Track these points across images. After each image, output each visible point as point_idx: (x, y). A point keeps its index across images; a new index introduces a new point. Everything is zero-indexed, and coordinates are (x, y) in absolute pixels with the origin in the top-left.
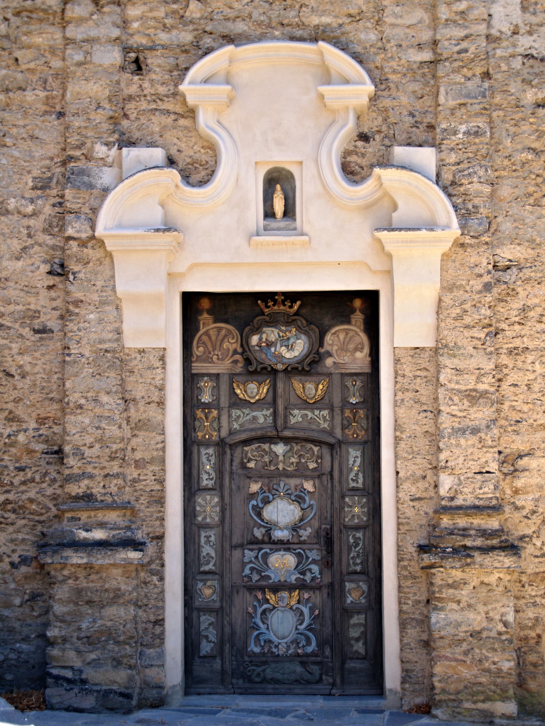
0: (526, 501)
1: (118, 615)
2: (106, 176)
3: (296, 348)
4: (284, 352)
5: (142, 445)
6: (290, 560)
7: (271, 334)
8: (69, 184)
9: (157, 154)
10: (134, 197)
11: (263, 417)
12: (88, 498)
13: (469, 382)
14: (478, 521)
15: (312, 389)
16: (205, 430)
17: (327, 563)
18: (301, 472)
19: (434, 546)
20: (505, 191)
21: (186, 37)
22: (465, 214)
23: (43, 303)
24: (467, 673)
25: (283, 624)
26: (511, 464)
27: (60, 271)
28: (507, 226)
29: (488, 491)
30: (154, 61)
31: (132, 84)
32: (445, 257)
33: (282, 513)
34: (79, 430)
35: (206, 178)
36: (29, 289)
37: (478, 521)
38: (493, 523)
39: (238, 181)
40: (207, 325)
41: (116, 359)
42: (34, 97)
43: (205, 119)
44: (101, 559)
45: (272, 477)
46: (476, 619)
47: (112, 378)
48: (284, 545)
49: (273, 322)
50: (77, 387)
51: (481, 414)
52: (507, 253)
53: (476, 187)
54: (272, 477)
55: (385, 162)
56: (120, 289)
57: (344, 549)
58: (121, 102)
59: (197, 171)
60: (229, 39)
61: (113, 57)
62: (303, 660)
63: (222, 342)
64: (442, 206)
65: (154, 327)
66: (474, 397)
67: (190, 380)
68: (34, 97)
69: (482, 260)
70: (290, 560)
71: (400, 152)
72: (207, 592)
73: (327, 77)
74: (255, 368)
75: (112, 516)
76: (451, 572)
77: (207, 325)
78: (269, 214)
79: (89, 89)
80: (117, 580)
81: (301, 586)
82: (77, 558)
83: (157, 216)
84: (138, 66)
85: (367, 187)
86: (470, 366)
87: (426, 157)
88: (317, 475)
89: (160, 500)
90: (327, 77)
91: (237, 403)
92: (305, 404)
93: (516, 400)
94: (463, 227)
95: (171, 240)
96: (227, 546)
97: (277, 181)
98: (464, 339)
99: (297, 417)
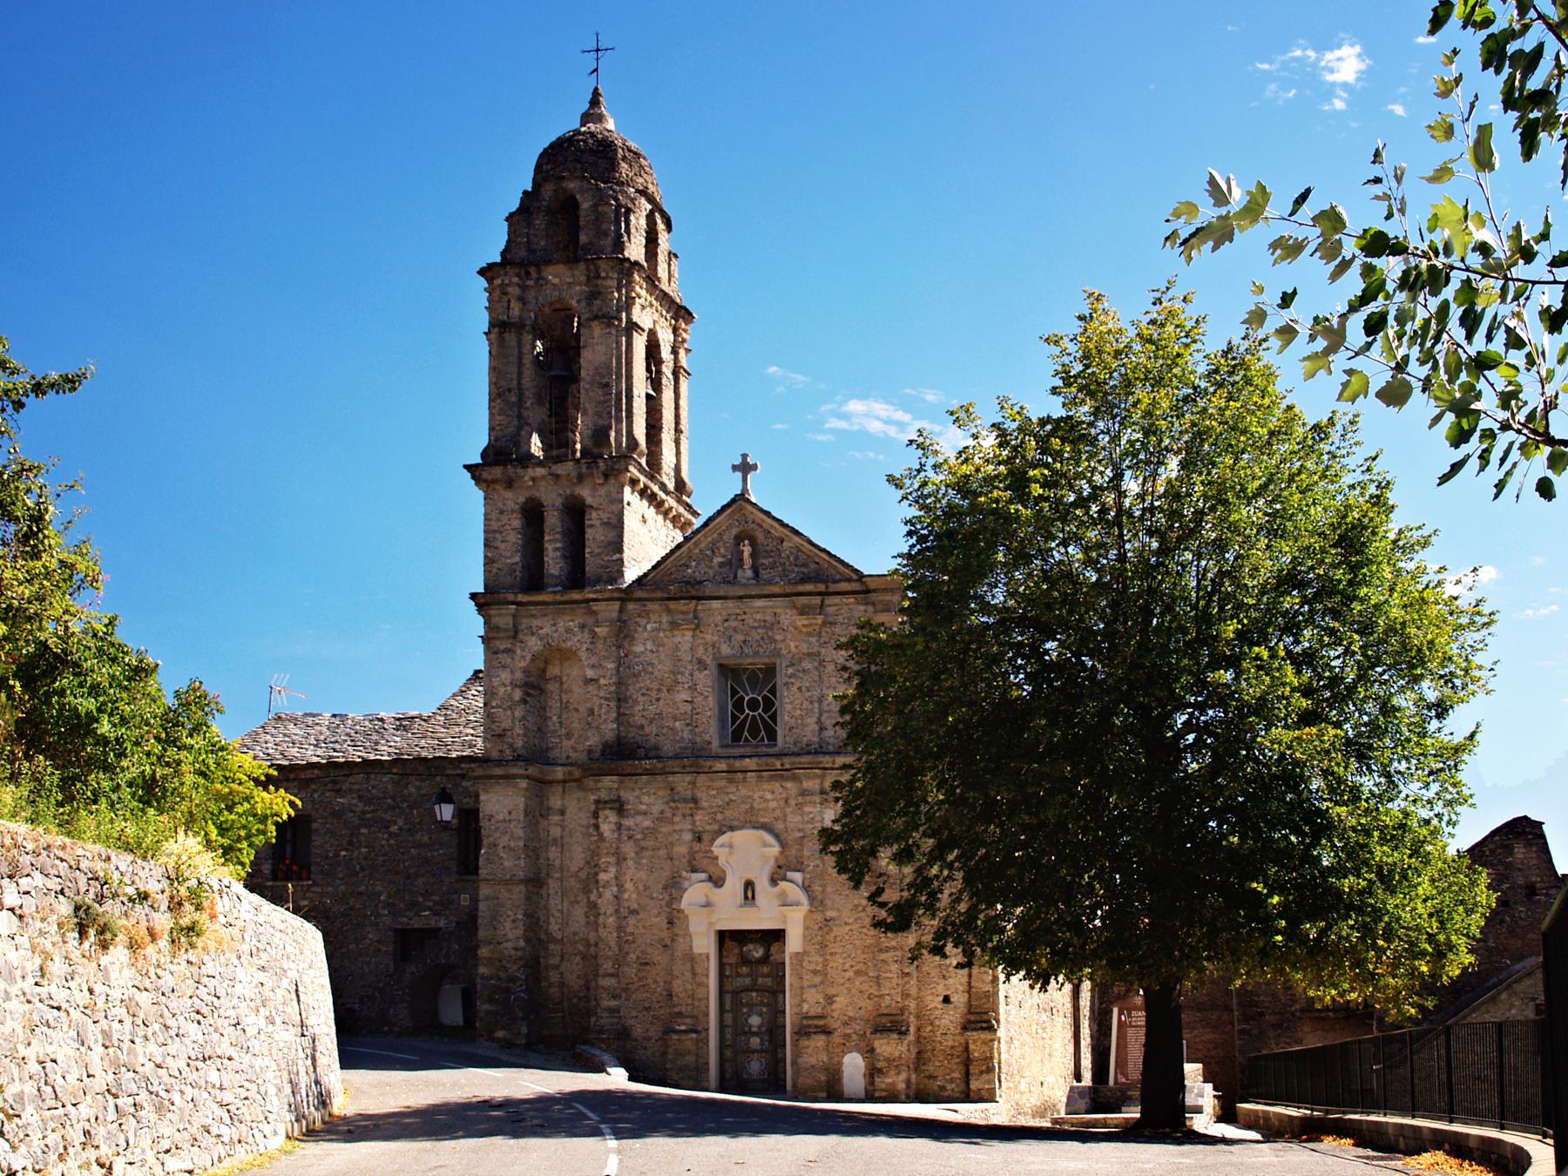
0: (835, 1014)
1: (690, 1059)
2: (686, 884)
3: (758, 953)
4: (749, 951)
5: (700, 993)
6: (758, 1040)
7: (751, 946)
8: (674, 887)
9: (703, 876)
10: (695, 892)
11: (748, 981)
12: (680, 1014)
13: (813, 967)
14: (816, 1022)
15: (766, 970)
16: (728, 987)
17: (771, 1041)
18: (762, 1004)
19: (803, 1032)
20: (829, 889)
21: (716, 827)
22: (812, 898)
23: (665, 934)
24: (809, 1081)
25: (755, 1067)
26: (830, 999)
27: (670, 923)
28: (829, 903)
29: (819, 1010)
30: (705, 837)
31: (697, 846)
32: (805, 918)
33: (755, 1021)
34: (677, 986)
35: (306, 1042)
36: (661, 930)
37: (816, 1022)
38: (821, 1023)
39: (734, 885)
40: (728, 943)
41: (691, 958)
42: (662, 852)
43: (721, 861)
44: (684, 1037)
45: (751, 1006)
46: (813, 1061)
47: (688, 966)
48: (756, 1034)
49: (751, 941)
50: (676, 971)
51: (817, 980)
52: (830, 914)
53: (817, 888)
54: (751, 1006)
55: (785, 879)
56: (692, 929)
57: (774, 1031)
58: (692, 854)
59: (717, 881)
60: (732, 829)
61: (688, 837)
62: (763, 1081)
63: (733, 949)
64: (801, 896)
65: (704, 944)
66: (815, 972)
67: (721, 966)
68: (662, 852)
69: (819, 917)
70: (758, 1040)
71: (790, 875)
72: (728, 1053)
73: (765, 845)
74: (745, 961)
75: (688, 1021)
76: (804, 1042)
77: (728, 943)
78: (746, 898)
79: (682, 850)
80: (690, 1045)
81: (762, 1051)
82: (675, 1037)
83: (703, 900)
84: (700, 839)
85: (777, 889)
86: (815, 961)
87: (798, 876)
88: (768, 1005)
89: (707, 1015)
90: (765, 845)
91: (739, 975)
92: (764, 976)
93: (832, 973)
94: (811, 905)
95: (709, 912)
96: (736, 1034)
97: (749, 885)
98: (811, 949)
99: (760, 980)
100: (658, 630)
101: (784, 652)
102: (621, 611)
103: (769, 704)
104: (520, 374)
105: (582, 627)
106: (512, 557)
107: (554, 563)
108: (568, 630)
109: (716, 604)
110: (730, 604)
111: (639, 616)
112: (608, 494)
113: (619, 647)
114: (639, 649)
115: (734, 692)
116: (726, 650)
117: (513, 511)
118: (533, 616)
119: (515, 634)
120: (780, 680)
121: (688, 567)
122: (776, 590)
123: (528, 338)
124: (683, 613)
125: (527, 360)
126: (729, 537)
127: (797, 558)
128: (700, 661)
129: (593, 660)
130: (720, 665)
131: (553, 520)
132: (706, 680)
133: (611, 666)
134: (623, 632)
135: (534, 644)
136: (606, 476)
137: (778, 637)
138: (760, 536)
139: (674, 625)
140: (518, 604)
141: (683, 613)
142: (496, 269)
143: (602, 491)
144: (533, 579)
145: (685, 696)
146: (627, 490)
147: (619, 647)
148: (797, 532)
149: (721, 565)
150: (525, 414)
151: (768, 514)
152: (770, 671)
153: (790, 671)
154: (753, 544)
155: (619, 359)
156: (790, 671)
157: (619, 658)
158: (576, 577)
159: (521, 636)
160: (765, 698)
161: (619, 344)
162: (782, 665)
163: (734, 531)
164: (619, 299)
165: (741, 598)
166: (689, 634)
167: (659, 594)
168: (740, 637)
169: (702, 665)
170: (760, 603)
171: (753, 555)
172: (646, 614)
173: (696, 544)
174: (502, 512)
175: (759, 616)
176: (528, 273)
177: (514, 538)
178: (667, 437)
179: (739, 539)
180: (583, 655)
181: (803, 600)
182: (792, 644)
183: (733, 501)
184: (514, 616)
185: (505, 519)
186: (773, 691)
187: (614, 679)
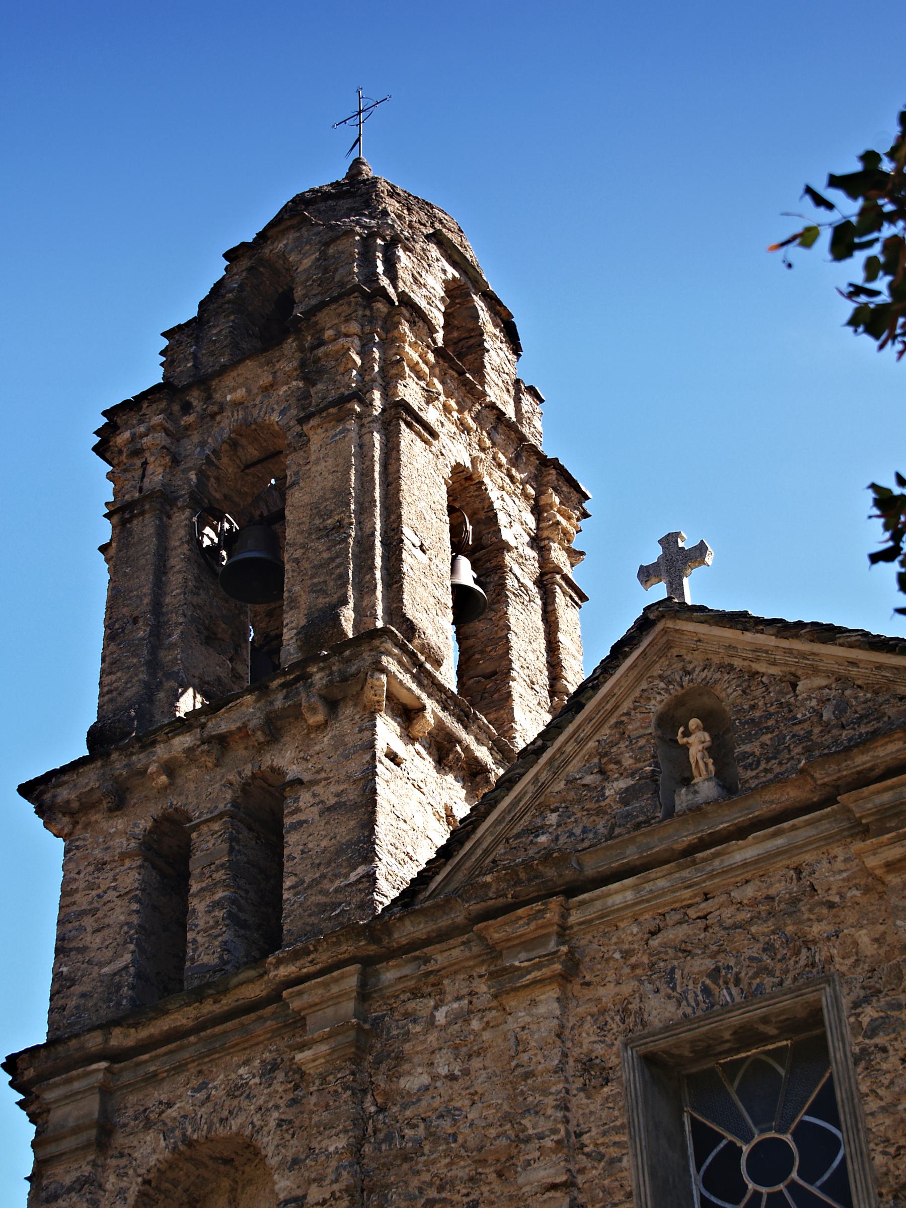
100: (465, 1017)
101: (841, 965)
102: (364, 994)
103: (819, 1148)
104: (159, 585)
105: (270, 1069)
106: (114, 957)
107: (207, 931)
108: (237, 1090)
109: (620, 894)
110: (660, 880)
111: (416, 994)
112: (339, 742)
113: (360, 1092)
114: (414, 1080)
115: (705, 1139)
116: (660, 1010)
117: (123, 856)
118: (153, 1079)
119: (104, 1133)
120: (842, 1046)
121: (536, 831)
122: (792, 795)
123: (181, 518)
124: (528, 944)
125: (178, 560)
126: (644, 725)
127: (841, 707)
128: (588, 1064)
129: (295, 1146)
130: (653, 1063)
131: (210, 844)
132: (606, 1114)
133: (337, 1144)
134: (370, 1045)
135: (150, 1150)
136: (333, 705)
137: (816, 930)
138: (729, 693)
139: (505, 982)
140: (115, 1056)
141: (528, 944)
142: (43, 1053)
143: (325, 740)
144: (162, 970)
145: (547, 1171)
146: (387, 732)
147: (360, 1092)
148: (827, 633)
149: (626, 797)
150: (166, 657)
151: (740, 620)
152: (807, 1037)
153: (869, 1013)
154: (713, 721)
155: (365, 475)
156: (869, 1013)
157: (360, 1121)
158: (261, 924)
159: (120, 1140)
160: (803, 1132)
161: (364, 450)
162: (839, 1006)
163: (656, 706)
164: (365, 369)
165: (690, 851)
166: (548, 1001)
167: (458, 915)
168: (701, 964)
169: (594, 1071)
170: (744, 852)
171: (718, 751)
172: (430, 985)
173: (556, 767)
174: (101, 866)
175: (749, 891)
176: (187, 408)
177: (121, 913)
178: (640, 1167)
179: (669, 722)
180: (268, 1142)
181: (878, 797)
182: (864, 937)
183: (644, 624)
184: (105, 1092)
185: (105, 880)
186: (826, 1106)
187: (346, 1178)
